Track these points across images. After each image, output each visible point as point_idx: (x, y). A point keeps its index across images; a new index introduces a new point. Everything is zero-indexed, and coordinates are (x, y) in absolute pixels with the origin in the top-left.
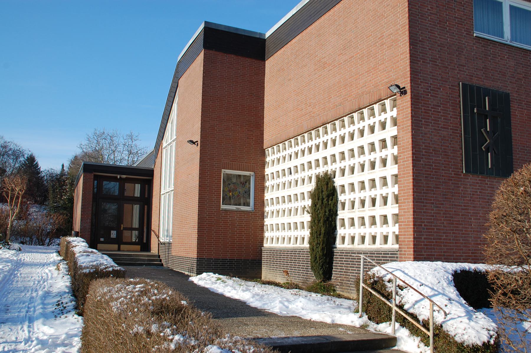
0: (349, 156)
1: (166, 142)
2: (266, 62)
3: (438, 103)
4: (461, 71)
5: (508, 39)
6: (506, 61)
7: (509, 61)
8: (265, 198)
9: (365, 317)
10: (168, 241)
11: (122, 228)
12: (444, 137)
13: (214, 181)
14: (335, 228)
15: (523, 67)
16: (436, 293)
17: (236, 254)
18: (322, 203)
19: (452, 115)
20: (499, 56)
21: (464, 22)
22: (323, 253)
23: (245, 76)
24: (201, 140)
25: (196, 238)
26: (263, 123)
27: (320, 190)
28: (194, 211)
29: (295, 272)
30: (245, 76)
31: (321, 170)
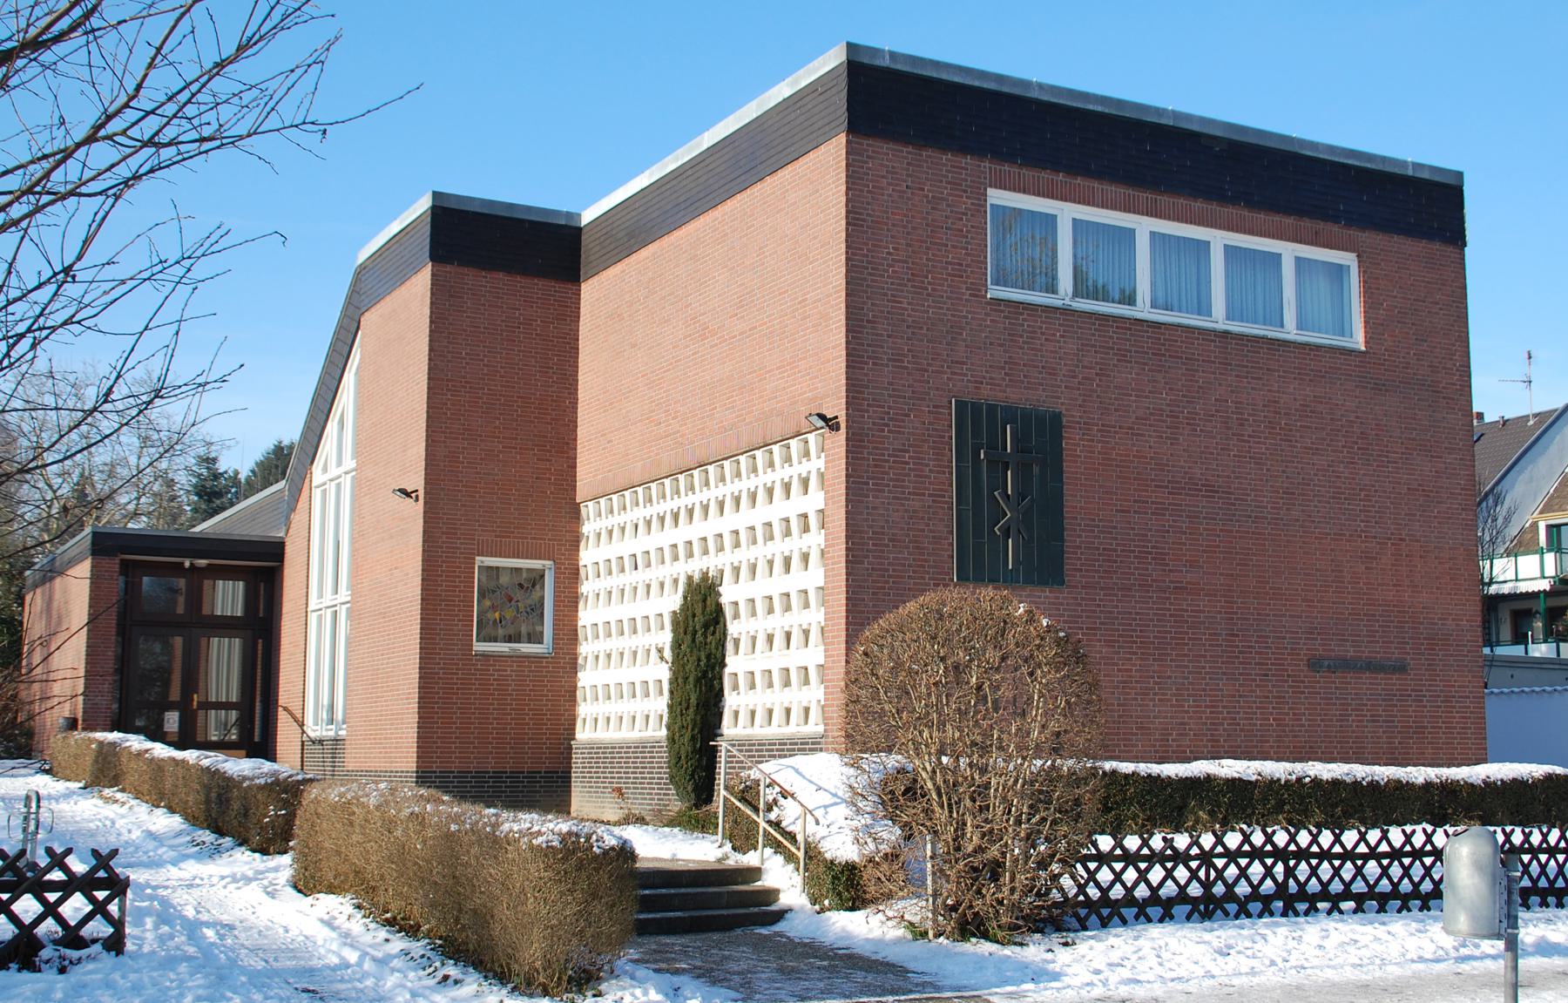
0: (748, 540)
1: (325, 470)
2: (583, 286)
3: (904, 445)
4: (955, 374)
5: (1066, 295)
6: (1059, 342)
7: (1065, 342)
8: (580, 624)
9: (728, 846)
10: (332, 733)
11: (195, 703)
12: (914, 511)
13: (457, 587)
14: (720, 694)
15: (1096, 352)
16: (839, 801)
17: (511, 758)
18: (693, 641)
19: (934, 466)
20: (1042, 334)
21: (966, 271)
22: (695, 747)
23: (532, 325)
24: (425, 488)
25: (414, 723)
26: (575, 440)
27: (689, 613)
28: (409, 660)
29: (644, 794)
30: (532, 325)
31: (696, 567)
